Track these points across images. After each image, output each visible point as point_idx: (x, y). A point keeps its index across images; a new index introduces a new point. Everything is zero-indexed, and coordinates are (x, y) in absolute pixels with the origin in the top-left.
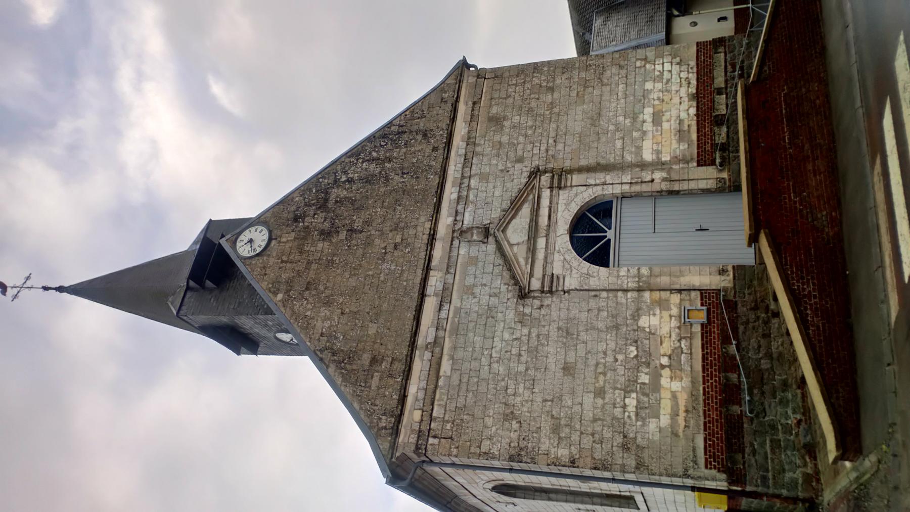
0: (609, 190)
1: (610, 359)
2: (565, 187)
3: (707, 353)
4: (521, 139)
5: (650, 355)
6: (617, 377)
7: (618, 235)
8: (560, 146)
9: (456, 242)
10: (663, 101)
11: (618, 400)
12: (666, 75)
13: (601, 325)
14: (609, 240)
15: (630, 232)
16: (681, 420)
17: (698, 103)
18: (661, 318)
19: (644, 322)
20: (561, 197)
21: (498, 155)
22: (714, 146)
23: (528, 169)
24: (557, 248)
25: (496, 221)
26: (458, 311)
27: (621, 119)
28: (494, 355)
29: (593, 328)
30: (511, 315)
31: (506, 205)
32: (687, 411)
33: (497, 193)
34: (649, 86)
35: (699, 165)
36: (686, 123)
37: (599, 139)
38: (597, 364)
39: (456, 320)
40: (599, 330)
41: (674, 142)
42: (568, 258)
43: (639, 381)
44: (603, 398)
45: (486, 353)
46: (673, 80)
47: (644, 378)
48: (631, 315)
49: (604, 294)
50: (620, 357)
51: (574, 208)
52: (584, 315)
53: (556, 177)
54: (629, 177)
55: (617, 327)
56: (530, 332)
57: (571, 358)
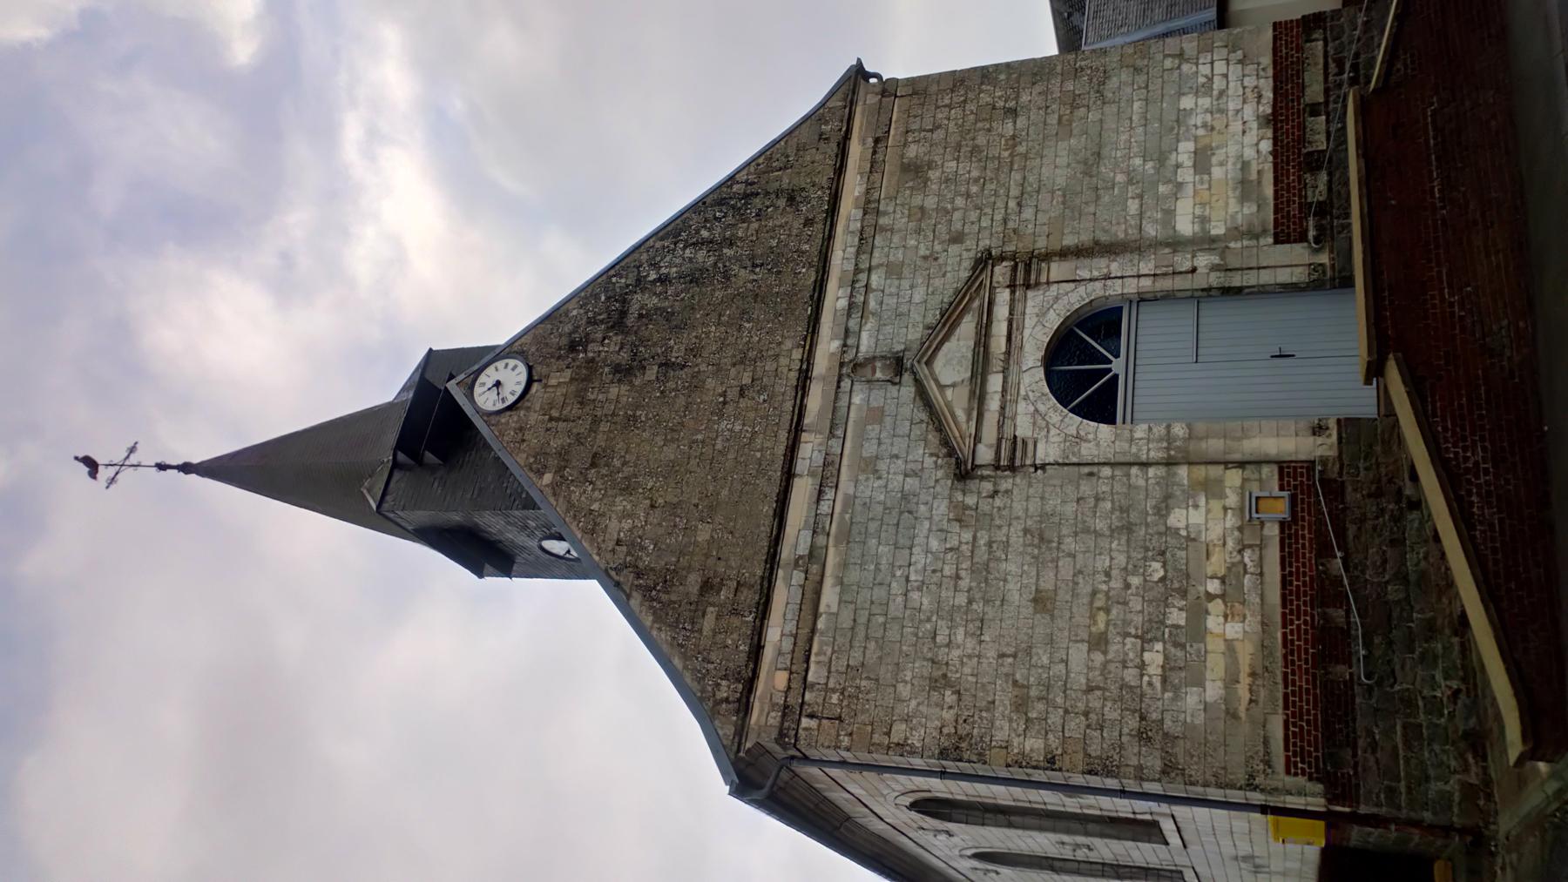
0: (1116, 288)
1: (1116, 584)
2: (1037, 284)
3: (1291, 573)
4: (960, 202)
5: (1188, 576)
6: (1129, 616)
7: (1133, 367)
8: (1028, 213)
9: (846, 384)
10: (1213, 129)
11: (1131, 655)
12: (1218, 84)
13: (1100, 525)
14: (1116, 377)
15: (1154, 361)
16: (1243, 691)
17: (1275, 132)
18: (1208, 511)
19: (1177, 518)
20: (1030, 303)
21: (919, 231)
22: (1305, 207)
23: (972, 254)
24: (1022, 392)
25: (916, 346)
26: (850, 501)
27: (1138, 161)
28: (912, 578)
29: (1087, 531)
30: (941, 508)
31: (932, 317)
32: (1253, 674)
33: (917, 298)
34: (1187, 102)
35: (1277, 241)
36: (1254, 167)
37: (1098, 198)
38: (1094, 593)
39: (847, 516)
40: (1097, 534)
41: (1232, 201)
42: (1042, 408)
43: (1169, 622)
44: (1105, 653)
45: (898, 573)
46: (1230, 92)
47: (1177, 617)
48: (1155, 507)
49: (1106, 471)
50: (1135, 581)
51: (1054, 321)
52: (1070, 508)
53: (1021, 267)
54: (1151, 265)
55: (1129, 528)
56: (975, 538)
57: (1047, 583)
